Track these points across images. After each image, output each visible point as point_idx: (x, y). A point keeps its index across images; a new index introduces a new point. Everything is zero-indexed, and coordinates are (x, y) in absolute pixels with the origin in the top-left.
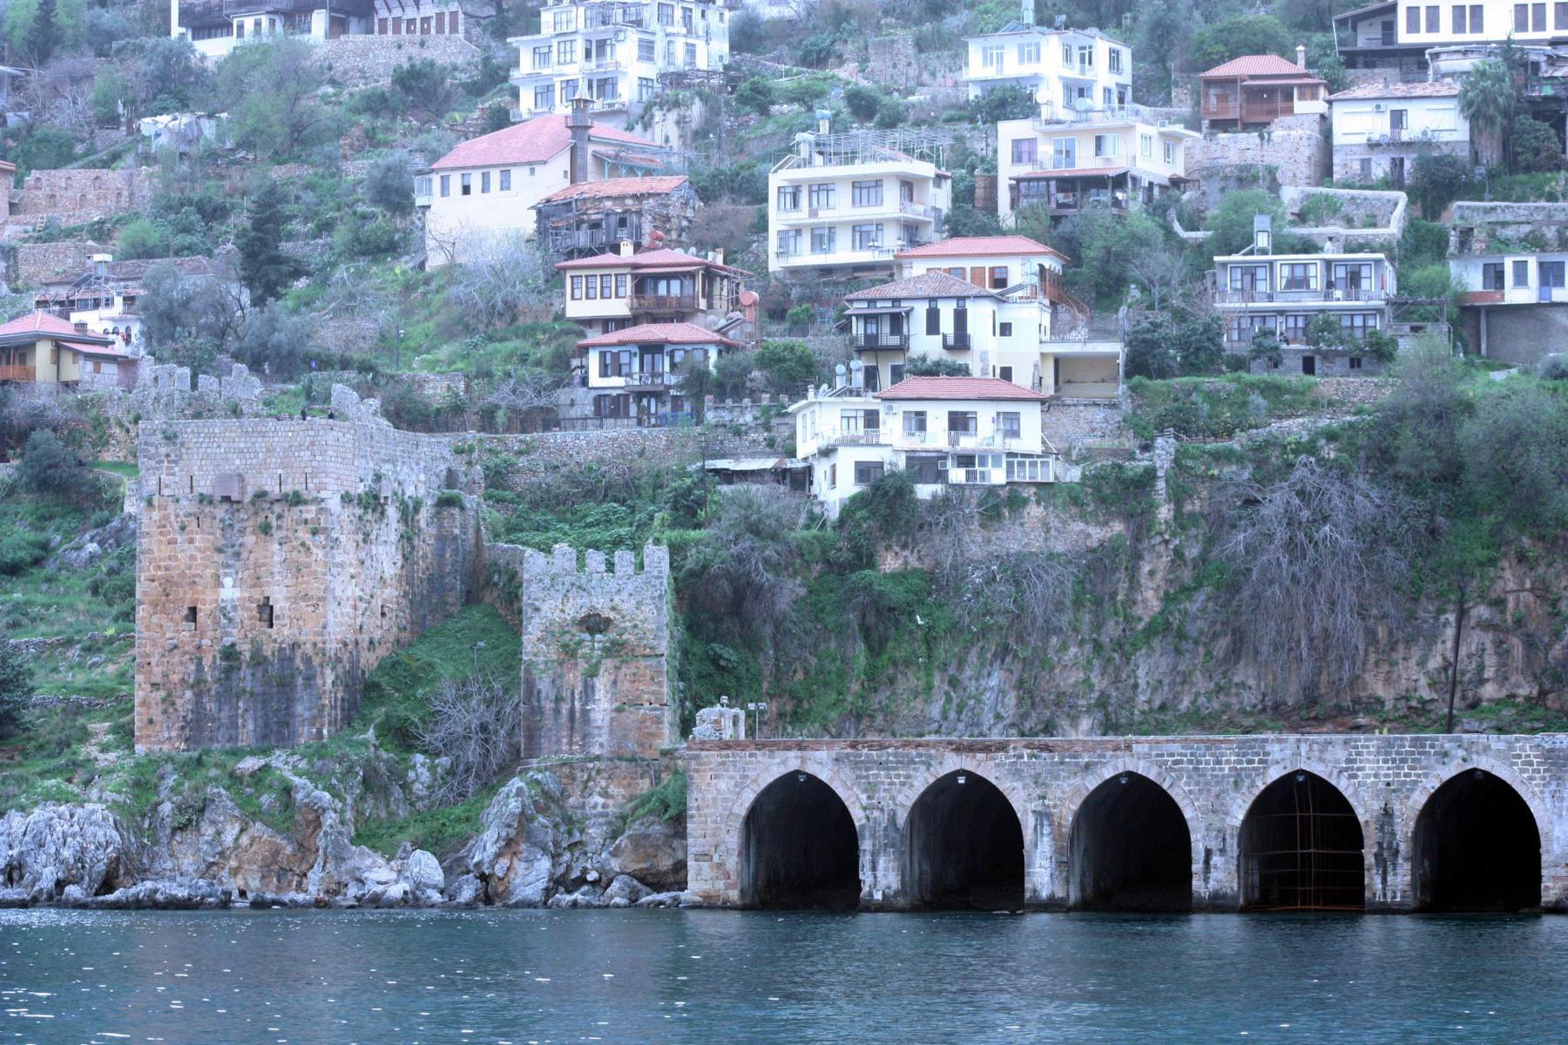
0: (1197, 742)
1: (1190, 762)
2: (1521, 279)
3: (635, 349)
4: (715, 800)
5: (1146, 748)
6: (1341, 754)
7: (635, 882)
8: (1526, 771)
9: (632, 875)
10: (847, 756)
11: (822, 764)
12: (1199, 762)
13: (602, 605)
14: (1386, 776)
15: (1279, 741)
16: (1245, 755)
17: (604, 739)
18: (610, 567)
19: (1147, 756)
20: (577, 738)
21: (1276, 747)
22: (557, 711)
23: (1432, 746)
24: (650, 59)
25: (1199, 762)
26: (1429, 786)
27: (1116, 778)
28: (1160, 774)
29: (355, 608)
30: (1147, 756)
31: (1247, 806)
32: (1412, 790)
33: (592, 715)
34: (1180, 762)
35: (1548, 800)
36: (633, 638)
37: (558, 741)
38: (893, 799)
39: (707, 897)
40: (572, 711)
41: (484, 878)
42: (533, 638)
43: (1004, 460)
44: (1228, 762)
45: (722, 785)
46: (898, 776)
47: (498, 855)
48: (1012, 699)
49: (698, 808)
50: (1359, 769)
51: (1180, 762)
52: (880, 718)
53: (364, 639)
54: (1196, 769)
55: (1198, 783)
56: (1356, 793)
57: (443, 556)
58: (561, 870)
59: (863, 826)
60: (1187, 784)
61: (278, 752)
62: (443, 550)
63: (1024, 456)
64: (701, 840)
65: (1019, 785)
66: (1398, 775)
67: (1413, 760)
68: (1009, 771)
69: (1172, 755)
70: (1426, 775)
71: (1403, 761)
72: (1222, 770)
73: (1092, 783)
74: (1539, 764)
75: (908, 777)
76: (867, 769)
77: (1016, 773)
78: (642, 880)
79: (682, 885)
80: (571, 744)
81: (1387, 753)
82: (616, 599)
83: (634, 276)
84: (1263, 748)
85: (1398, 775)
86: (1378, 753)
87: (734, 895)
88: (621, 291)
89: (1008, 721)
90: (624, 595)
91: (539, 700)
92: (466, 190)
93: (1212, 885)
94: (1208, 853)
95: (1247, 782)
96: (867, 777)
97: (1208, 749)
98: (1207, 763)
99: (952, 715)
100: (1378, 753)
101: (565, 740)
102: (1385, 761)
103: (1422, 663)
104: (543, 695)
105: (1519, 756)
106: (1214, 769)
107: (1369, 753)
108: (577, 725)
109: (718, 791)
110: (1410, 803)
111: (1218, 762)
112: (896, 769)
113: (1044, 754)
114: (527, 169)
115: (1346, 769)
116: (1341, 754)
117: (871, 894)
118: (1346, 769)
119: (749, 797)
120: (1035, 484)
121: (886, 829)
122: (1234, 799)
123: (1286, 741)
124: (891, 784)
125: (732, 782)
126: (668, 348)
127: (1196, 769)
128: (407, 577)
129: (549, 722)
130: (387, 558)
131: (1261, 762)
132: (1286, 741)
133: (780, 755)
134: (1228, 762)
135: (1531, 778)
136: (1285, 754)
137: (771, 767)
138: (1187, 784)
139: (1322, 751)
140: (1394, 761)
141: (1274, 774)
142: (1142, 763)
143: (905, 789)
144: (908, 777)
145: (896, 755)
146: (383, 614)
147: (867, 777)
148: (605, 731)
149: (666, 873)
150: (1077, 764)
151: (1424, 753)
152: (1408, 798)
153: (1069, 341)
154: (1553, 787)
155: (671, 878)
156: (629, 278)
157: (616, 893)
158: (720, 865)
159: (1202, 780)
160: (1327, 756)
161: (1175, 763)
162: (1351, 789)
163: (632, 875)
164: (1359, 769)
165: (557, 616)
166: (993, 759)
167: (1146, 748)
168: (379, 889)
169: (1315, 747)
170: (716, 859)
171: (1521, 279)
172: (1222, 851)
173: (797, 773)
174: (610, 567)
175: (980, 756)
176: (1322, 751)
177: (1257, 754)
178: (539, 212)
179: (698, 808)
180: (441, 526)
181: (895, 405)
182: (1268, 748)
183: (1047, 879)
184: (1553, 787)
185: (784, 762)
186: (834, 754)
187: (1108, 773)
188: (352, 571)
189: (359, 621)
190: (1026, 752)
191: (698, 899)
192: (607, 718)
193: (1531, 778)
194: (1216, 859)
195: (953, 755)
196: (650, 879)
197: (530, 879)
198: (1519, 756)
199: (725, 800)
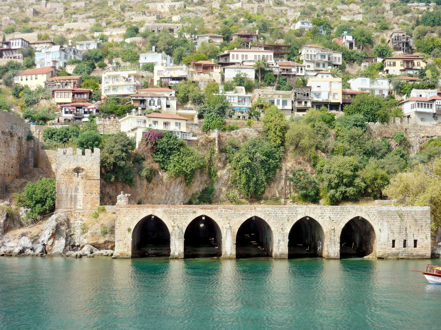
0: (276, 207)
1: (274, 213)
2: (278, 103)
3: (75, 108)
4: (124, 223)
5: (260, 209)
6: (320, 212)
7: (92, 247)
8: (373, 217)
9: (91, 245)
10: (167, 210)
11: (159, 212)
12: (277, 213)
13: (80, 164)
14: (333, 218)
15: (301, 207)
16: (290, 211)
17: (81, 204)
18: (83, 154)
19: (261, 211)
20: (73, 203)
21: (300, 209)
22: (67, 195)
23: (346, 209)
24: (67, 59)
25: (277, 213)
26: (345, 221)
27: (252, 218)
28: (265, 217)
29: (4, 164)
30: (261, 211)
31: (291, 227)
32: (340, 222)
33: (78, 197)
34: (271, 213)
35: (380, 225)
36: (90, 174)
37: (67, 204)
38: (182, 224)
39: (122, 254)
40: (71, 196)
41: (44, 245)
42: (60, 174)
43: (180, 133)
44: (286, 213)
45: (127, 219)
46: (183, 217)
47: (49, 239)
48: (182, 194)
49: (119, 226)
50: (325, 216)
51: (271, 213)
52: (150, 199)
53: (7, 173)
54: (276, 216)
55: (276, 220)
56: (324, 223)
57: (28, 153)
58: (68, 242)
59: (172, 232)
60: (273, 220)
61: (119, 196)
62: (29, 151)
63: (184, 133)
64: (120, 236)
65: (221, 220)
66: (336, 218)
67: (340, 213)
68: (218, 216)
69: (269, 211)
70: (344, 218)
71: (338, 214)
72: (283, 216)
73: (244, 219)
74: (377, 215)
75: (187, 217)
76: (174, 214)
77: (220, 216)
78: (94, 246)
79: (113, 248)
80: (71, 205)
81: (333, 211)
82: (86, 163)
83: (73, 93)
84: (296, 209)
85: (336, 218)
86: (330, 211)
87: (130, 253)
88: (69, 96)
89: (181, 200)
90: (88, 162)
91: (61, 192)
92: (27, 80)
93: (280, 251)
94: (279, 241)
95: (291, 220)
96: (173, 217)
97: (280, 209)
98: (279, 214)
99: (167, 199)
100: (330, 211)
101: (69, 204)
102: (333, 214)
103: (277, 188)
104: (62, 191)
105: (371, 213)
106: (281, 216)
107: (328, 211)
108: (73, 199)
109: (126, 221)
110: (340, 226)
111: (282, 214)
112: (183, 214)
113: (229, 211)
114: (41, 75)
115: (321, 216)
116: (320, 212)
117: (174, 253)
118: (321, 216)
119: (136, 222)
120: (187, 140)
121: (179, 233)
122: (287, 225)
123: (303, 207)
124: (181, 219)
125: (130, 218)
126: (83, 108)
127: (276, 216)
128: (19, 157)
129: (64, 199)
130: (14, 153)
131: (295, 213)
132: (303, 207)
133: (146, 210)
134: (286, 213)
135: (375, 219)
136: (200, 211)
137: (144, 212)
138: (273, 220)
139: (313, 211)
140: (335, 214)
141: (299, 217)
142: (259, 213)
143: (185, 220)
144: (187, 217)
145: (183, 210)
146: (12, 167)
147: (173, 217)
148: (82, 201)
149: (102, 244)
150: (239, 214)
151: (344, 211)
152: (339, 225)
153: (186, 109)
154: (381, 222)
155: (103, 246)
156: (71, 93)
157: (86, 250)
158: (126, 244)
159: (277, 219)
160: (315, 212)
161: (270, 213)
162: (322, 222)
163: (91, 245)
164: (325, 216)
165: (67, 168)
166: (213, 212)
167: (260, 209)
168: (12, 249)
169: (312, 209)
170: (124, 242)
171: (278, 103)
172: (284, 240)
173: (151, 215)
174: (83, 154)
175: (209, 210)
176: (313, 211)
177: (294, 211)
178: (45, 83)
179: (119, 226)
180: (28, 145)
181: (151, 118)
182: (298, 209)
183: (230, 248)
184: (381, 222)
185: (147, 212)
186: (163, 209)
187: (249, 217)
188: (4, 153)
189: (5, 168)
190: (223, 210)
191: (118, 254)
192: (82, 198)
193: (375, 219)
194: (282, 243)
195: (201, 210)
196: (96, 246)
197: (59, 245)
198: (371, 213)
199: (128, 223)
